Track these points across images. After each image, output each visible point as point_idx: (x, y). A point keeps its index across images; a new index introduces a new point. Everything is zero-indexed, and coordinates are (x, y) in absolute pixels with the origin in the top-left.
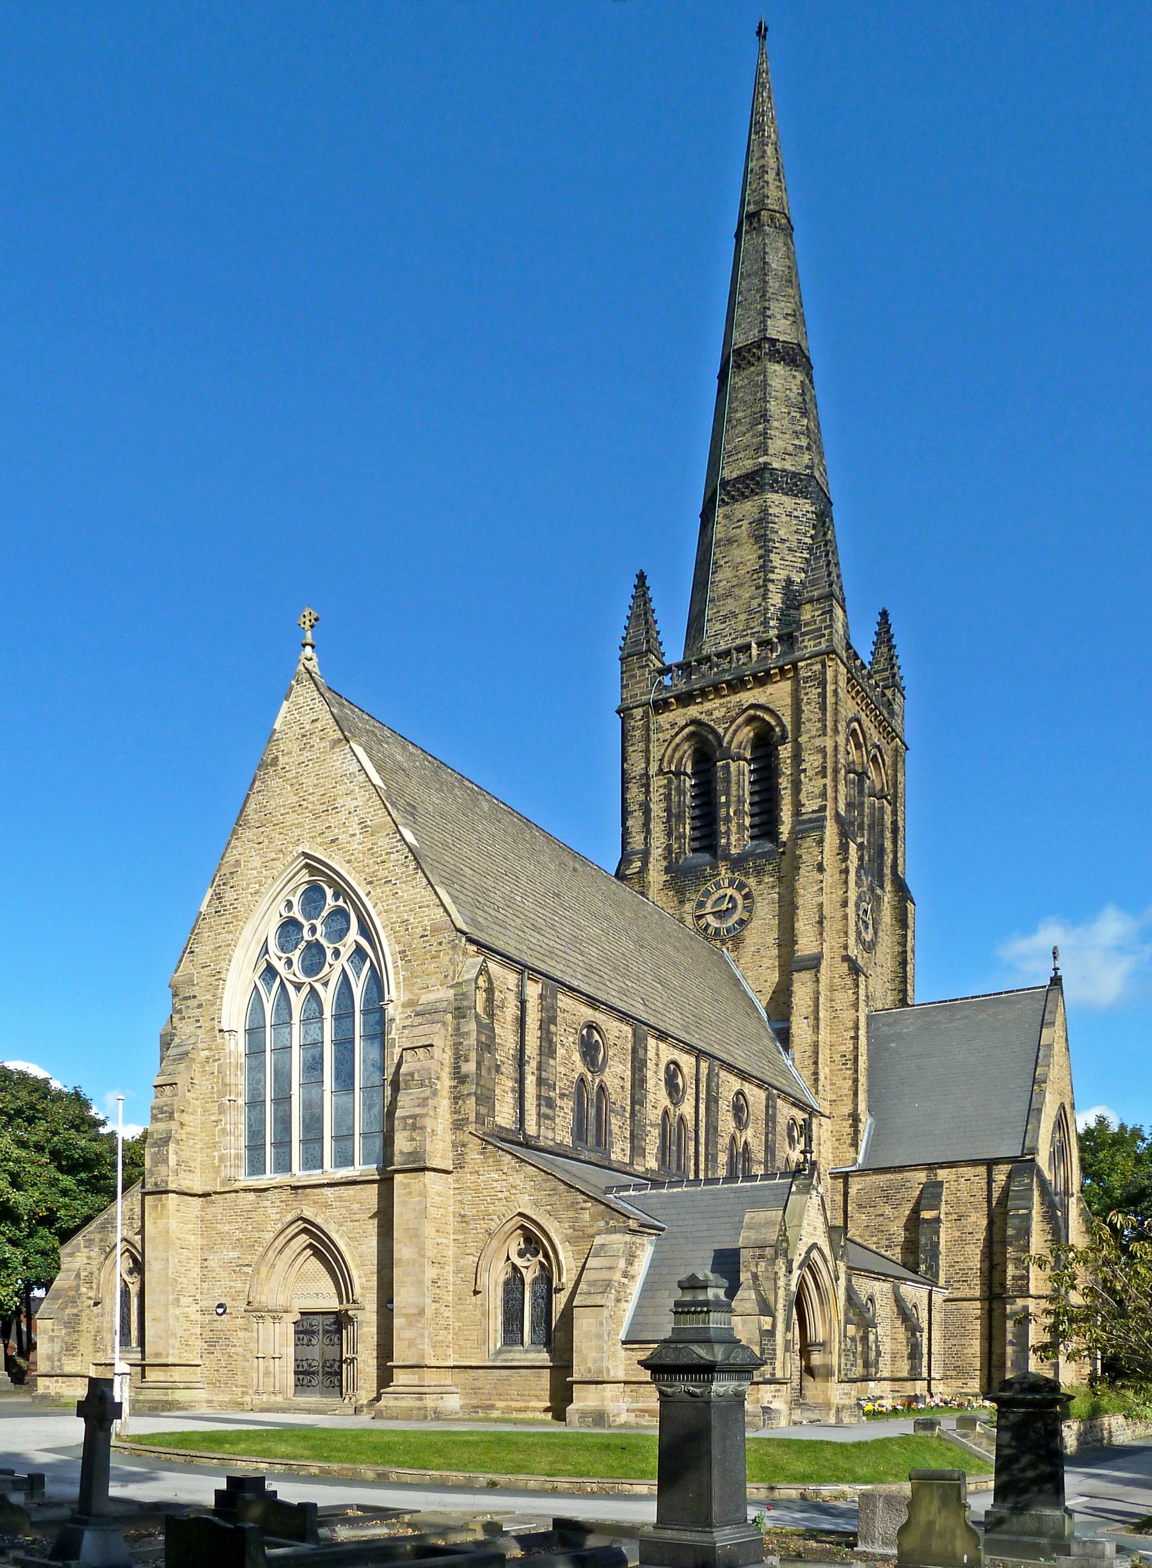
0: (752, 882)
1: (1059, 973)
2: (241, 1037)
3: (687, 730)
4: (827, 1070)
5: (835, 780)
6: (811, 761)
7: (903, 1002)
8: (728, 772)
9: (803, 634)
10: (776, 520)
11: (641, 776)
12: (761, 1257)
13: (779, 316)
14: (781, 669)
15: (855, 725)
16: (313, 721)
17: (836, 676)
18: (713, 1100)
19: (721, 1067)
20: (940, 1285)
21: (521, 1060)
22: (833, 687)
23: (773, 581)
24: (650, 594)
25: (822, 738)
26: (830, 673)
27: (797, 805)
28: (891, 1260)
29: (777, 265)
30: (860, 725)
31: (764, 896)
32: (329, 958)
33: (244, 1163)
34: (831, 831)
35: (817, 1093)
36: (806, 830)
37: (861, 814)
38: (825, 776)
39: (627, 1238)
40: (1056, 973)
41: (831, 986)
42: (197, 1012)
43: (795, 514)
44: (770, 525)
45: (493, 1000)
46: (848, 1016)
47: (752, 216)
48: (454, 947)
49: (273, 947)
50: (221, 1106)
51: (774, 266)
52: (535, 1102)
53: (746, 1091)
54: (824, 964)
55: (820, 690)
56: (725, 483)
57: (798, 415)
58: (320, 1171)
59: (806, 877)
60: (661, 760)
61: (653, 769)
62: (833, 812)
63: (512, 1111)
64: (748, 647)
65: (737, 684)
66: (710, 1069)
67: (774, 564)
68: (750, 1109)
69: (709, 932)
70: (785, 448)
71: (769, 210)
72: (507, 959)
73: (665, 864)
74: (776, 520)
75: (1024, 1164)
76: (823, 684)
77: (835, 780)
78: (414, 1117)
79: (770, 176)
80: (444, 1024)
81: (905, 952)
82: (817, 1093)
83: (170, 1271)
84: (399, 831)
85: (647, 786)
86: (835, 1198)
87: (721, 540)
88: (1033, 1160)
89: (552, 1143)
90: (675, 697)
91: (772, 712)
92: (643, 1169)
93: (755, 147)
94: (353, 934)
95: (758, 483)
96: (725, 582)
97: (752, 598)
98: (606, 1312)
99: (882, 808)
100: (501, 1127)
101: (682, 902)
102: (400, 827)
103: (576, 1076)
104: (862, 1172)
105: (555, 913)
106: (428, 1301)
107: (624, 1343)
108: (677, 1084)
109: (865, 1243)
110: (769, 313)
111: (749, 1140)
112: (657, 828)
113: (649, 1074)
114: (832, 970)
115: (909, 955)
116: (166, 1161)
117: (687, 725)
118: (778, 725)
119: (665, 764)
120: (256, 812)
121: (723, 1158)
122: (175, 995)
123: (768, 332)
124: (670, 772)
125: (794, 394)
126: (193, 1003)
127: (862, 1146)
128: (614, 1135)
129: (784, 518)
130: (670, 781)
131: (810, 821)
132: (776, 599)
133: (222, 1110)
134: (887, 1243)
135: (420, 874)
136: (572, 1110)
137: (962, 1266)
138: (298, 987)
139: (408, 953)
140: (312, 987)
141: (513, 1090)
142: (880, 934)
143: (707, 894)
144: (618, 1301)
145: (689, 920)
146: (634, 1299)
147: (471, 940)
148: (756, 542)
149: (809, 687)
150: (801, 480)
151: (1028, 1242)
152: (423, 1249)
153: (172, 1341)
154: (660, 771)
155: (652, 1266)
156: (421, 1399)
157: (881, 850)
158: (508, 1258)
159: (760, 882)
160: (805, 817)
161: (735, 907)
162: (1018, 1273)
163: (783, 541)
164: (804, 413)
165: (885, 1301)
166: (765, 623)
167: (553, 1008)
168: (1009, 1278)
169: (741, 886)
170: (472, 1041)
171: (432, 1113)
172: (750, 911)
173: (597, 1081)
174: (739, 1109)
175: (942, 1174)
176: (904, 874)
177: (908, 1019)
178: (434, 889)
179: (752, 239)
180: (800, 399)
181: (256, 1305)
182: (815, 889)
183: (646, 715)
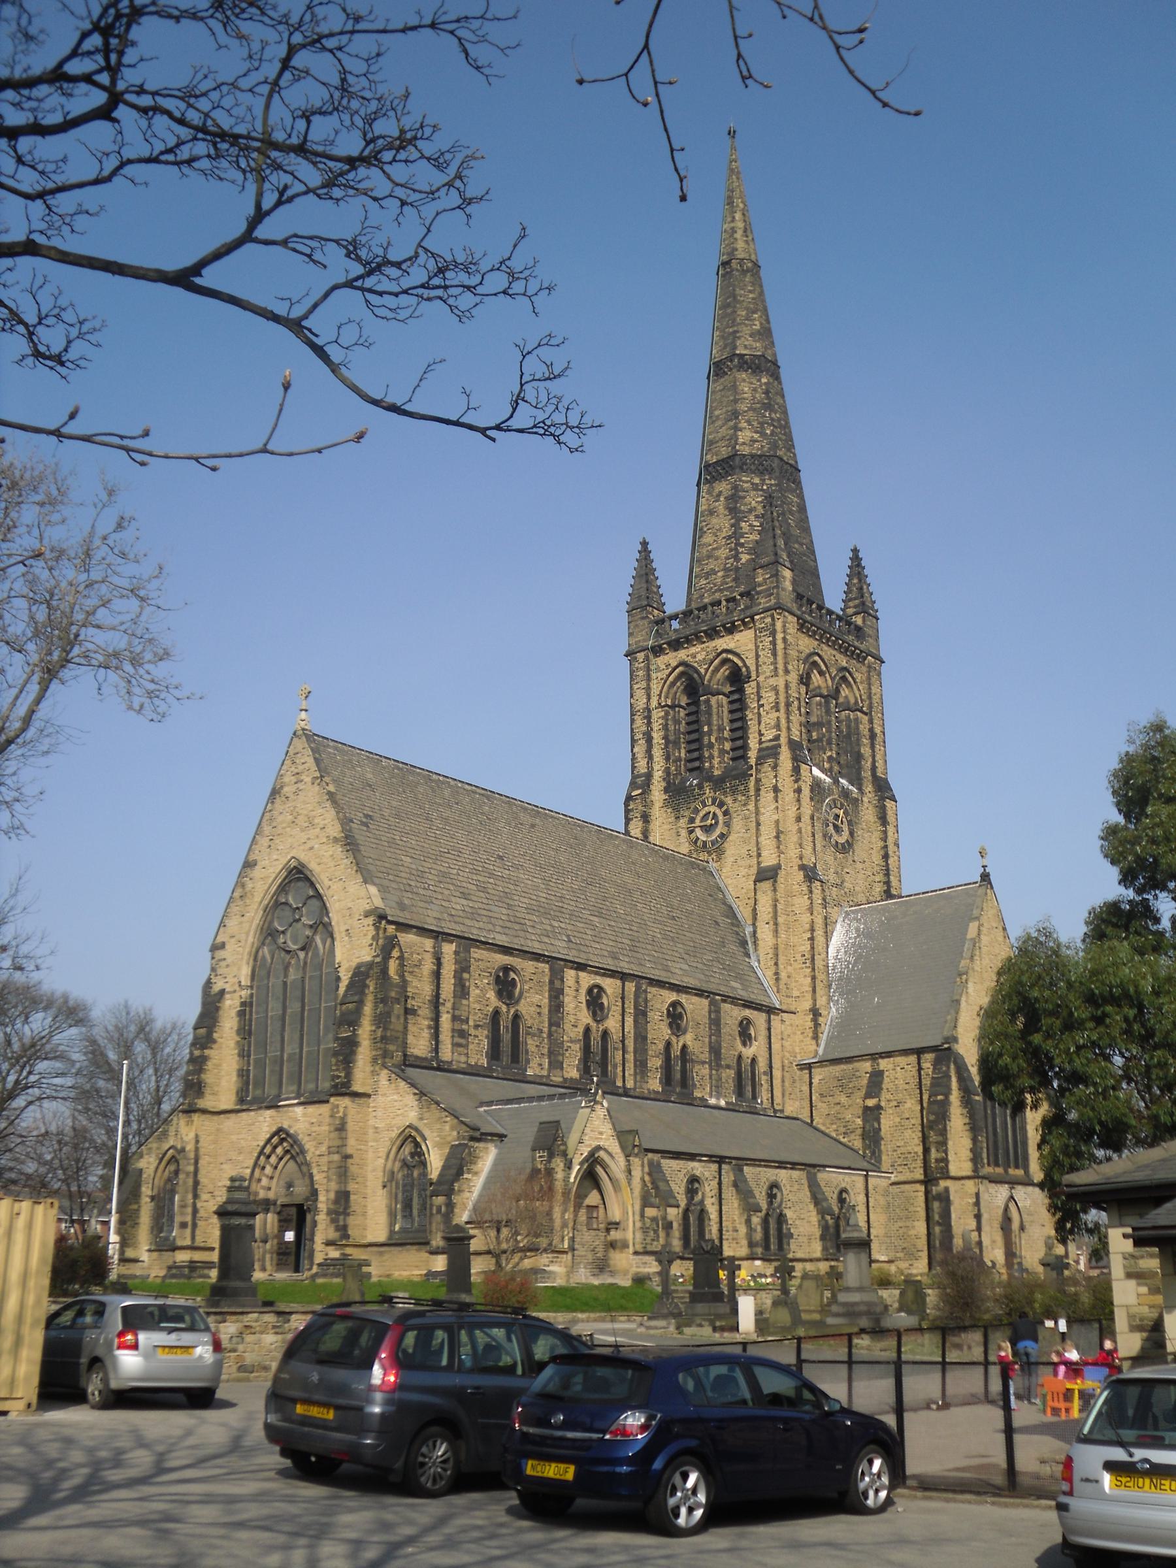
0: (729, 800)
3: (677, 671)
6: (768, 697)
8: (709, 706)
9: (758, 593)
11: (644, 709)
15: (817, 658)
18: (641, 1014)
22: (782, 635)
38: (778, 710)
46: (806, 918)
53: (683, 1001)
61: (654, 703)
63: (427, 1043)
64: (719, 603)
65: (712, 634)
66: (638, 988)
72: (422, 931)
76: (773, 633)
77: (788, 713)
81: (886, 847)
85: (648, 718)
88: (949, 1049)
89: (464, 1066)
92: (561, 1079)
97: (728, 558)
99: (856, 719)
104: (822, 1063)
112: (657, 753)
113: (566, 1000)
115: (891, 849)
117: (677, 667)
121: (655, 1063)
124: (667, 705)
126: (223, 964)
127: (823, 1038)
130: (667, 713)
131: (768, 748)
136: (487, 1037)
137: (903, 1150)
141: (429, 1027)
143: (696, 811)
145: (684, 833)
154: (660, 706)
157: (859, 757)
160: (764, 745)
161: (717, 823)
165: (796, 1187)
169: (721, 804)
172: (728, 826)
173: (512, 1011)
174: (675, 1017)
175: (884, 1064)
183: (647, 658)
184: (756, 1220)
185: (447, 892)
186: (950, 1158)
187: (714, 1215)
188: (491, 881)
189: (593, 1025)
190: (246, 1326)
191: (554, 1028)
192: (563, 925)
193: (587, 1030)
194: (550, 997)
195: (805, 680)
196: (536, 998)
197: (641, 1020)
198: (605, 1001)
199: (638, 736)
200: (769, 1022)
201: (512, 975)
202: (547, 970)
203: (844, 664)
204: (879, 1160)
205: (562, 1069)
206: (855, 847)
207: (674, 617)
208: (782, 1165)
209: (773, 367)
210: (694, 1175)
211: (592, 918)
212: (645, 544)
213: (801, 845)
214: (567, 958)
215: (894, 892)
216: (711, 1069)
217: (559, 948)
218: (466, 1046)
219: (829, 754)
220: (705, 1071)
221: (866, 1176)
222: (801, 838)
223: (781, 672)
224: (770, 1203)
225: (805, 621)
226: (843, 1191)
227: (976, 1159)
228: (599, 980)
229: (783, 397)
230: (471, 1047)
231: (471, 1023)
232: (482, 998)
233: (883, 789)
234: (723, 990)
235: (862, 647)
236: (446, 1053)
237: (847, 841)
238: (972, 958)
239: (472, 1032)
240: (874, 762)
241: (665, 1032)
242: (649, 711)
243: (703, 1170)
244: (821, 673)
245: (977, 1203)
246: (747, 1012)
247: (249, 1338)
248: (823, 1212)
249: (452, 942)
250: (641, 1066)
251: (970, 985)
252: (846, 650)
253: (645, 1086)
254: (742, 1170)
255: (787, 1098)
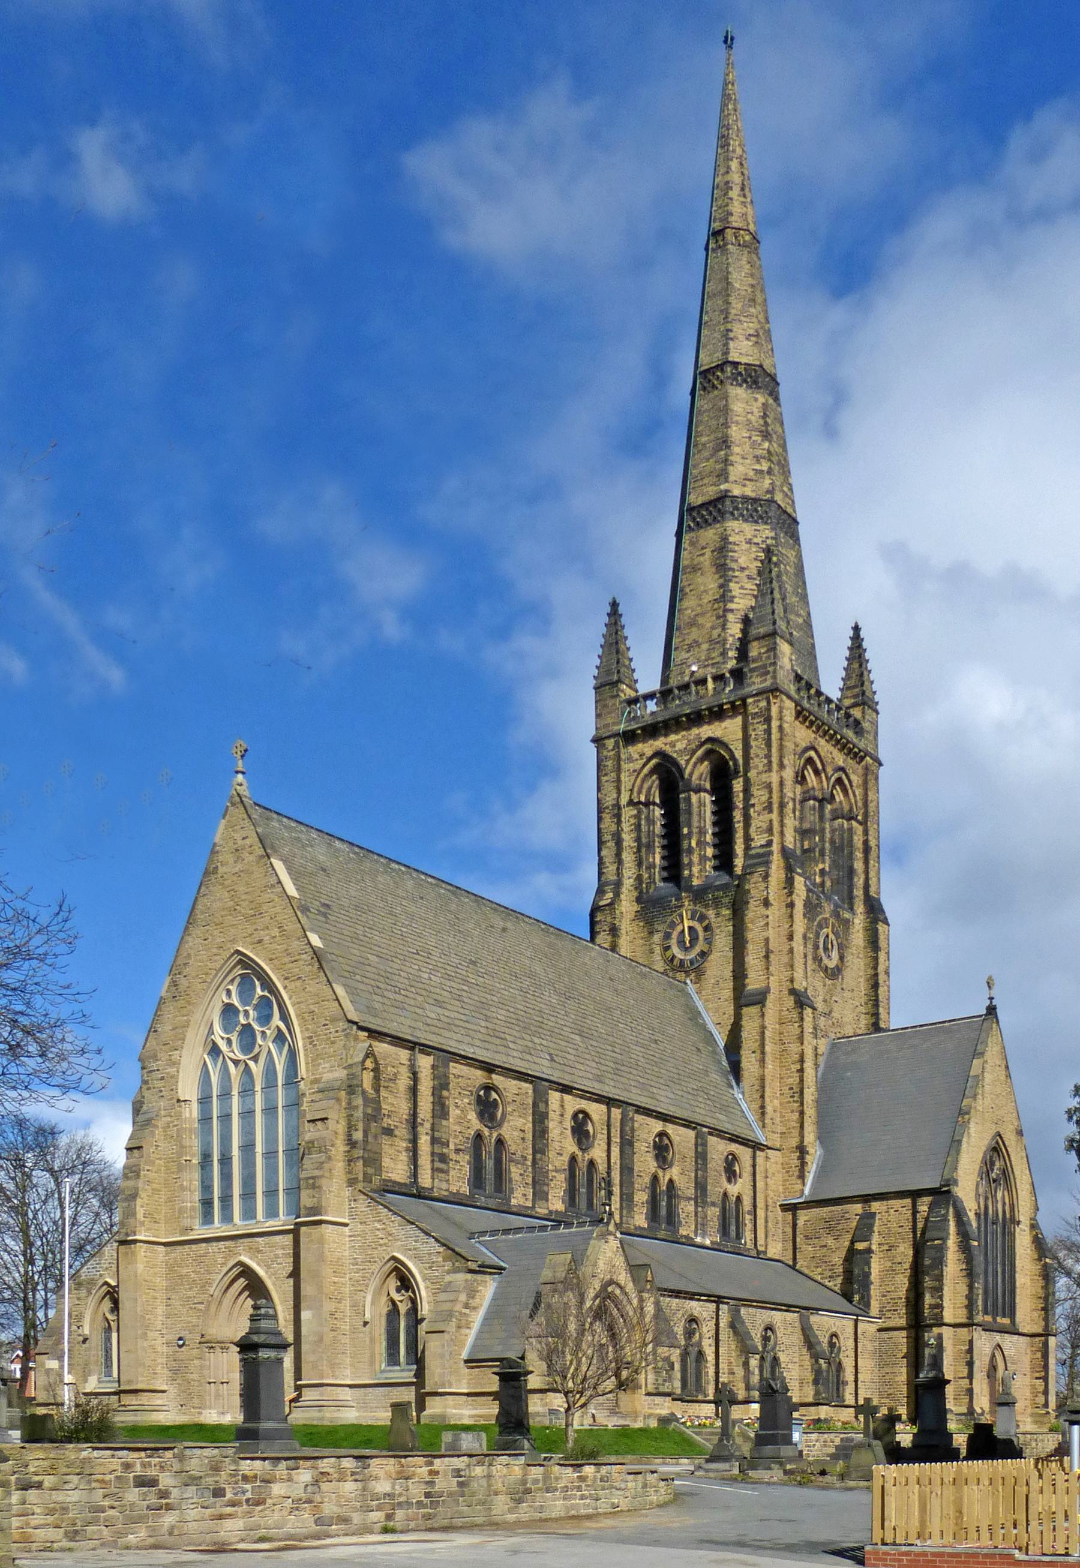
0: (711, 913)
1: (994, 1002)
2: (195, 1106)
4: (776, 1102)
5: (782, 815)
6: (759, 796)
7: (876, 1027)
9: (752, 670)
10: (736, 548)
11: (613, 805)
12: (555, 1291)
13: (741, 338)
14: (732, 703)
15: (812, 753)
16: (244, 838)
17: (781, 712)
18: (627, 1144)
19: (637, 1112)
20: (872, 1314)
21: (413, 1122)
22: (778, 723)
23: (732, 611)
24: (623, 620)
25: (767, 775)
26: (774, 710)
27: (747, 839)
28: (832, 1290)
29: (740, 284)
30: (817, 752)
31: (723, 928)
32: (259, 1041)
33: (198, 1214)
34: (777, 861)
35: (764, 1127)
36: (754, 865)
37: (822, 839)
39: (469, 1276)
40: (991, 1002)
41: (780, 1019)
42: (161, 1084)
43: (755, 540)
44: (730, 554)
45: (379, 1079)
46: (794, 1048)
47: (718, 234)
48: (346, 1035)
49: (217, 1028)
50: (180, 1164)
51: (737, 285)
52: (429, 1158)
53: (670, 1132)
54: (771, 998)
55: (765, 727)
56: (691, 509)
57: (759, 439)
58: (254, 1221)
59: (753, 911)
60: (631, 790)
61: (624, 799)
62: (780, 846)
63: (406, 1168)
64: (703, 682)
65: (696, 719)
67: (734, 593)
68: (675, 1147)
69: (675, 963)
70: (746, 474)
71: (733, 228)
72: (398, 1041)
73: (636, 894)
74: (736, 548)
75: (942, 1194)
76: (768, 720)
77: (782, 815)
78: (313, 1178)
79: (734, 193)
80: (338, 1100)
81: (876, 975)
82: (764, 1127)
83: (139, 1309)
84: (306, 936)
85: (618, 816)
86: (785, 1230)
87: (686, 567)
88: (949, 1192)
89: (446, 1193)
90: (642, 728)
91: (726, 746)
92: (546, 1212)
93: (721, 161)
94: (276, 1021)
95: (719, 510)
96: (690, 611)
98: (446, 1336)
99: (850, 829)
100: (395, 1182)
101: (651, 933)
102: (308, 933)
103: (473, 1133)
105: (465, 981)
106: (326, 1329)
107: (466, 1361)
108: (588, 1131)
109: (811, 1274)
110: (731, 335)
111: (675, 1178)
112: (628, 857)
113: (551, 1125)
114: (777, 1005)
115: (882, 978)
116: (134, 1214)
118: (731, 759)
119: (635, 794)
120: (203, 913)
121: (641, 1197)
122: (143, 1068)
123: (731, 354)
124: (640, 802)
125: (755, 418)
127: (810, 1178)
128: (514, 1183)
129: (745, 546)
130: (640, 812)
131: (759, 855)
132: (735, 629)
133: (180, 1169)
134: (830, 1274)
135: (322, 974)
136: (469, 1163)
138: (236, 1062)
139: (314, 1039)
140: (246, 1065)
141: (407, 1149)
142: (849, 958)
144: (459, 1327)
145: (658, 950)
146: (476, 1326)
147: (362, 1028)
148: (717, 572)
149: (758, 723)
150: (761, 506)
151: (942, 1272)
152: (321, 1286)
153: (140, 1370)
154: (631, 803)
155: (494, 1299)
156: (320, 1411)
157: (851, 872)
158: (389, 1294)
159: (718, 915)
160: (753, 852)
162: (933, 1302)
163: (742, 569)
164: (766, 435)
165: (790, 1330)
166: (724, 654)
167: (446, 1076)
168: (927, 1306)
169: (702, 918)
170: (359, 1114)
171: (327, 1174)
173: (495, 1135)
174: (662, 1149)
175: (876, 1206)
176: (879, 893)
177: (865, 1047)
178: (332, 987)
179: (717, 257)
180: (762, 422)
181: (207, 1338)
182: (762, 924)
183: (617, 745)
184: (754, 1362)
185: (420, 998)
186: (945, 1304)
187: (710, 1357)
188: (466, 988)
189: (579, 1153)
190: (322, 1473)
191: (538, 1156)
192: (544, 1042)
193: (573, 1159)
194: (534, 1122)
195: (800, 779)
196: (519, 1122)
197: (627, 1148)
198: (590, 1128)
199: (607, 837)
200: (754, 1157)
201: (494, 1095)
202: (530, 1091)
203: (841, 763)
204: (868, 1305)
205: (547, 1200)
206: (844, 973)
207: (650, 696)
208: (777, 1306)
209: (772, 384)
210: (692, 1315)
211: (573, 1036)
212: (856, 629)
213: (792, 966)
214: (552, 1078)
215: (882, 1025)
216: (696, 1206)
217: (543, 1068)
218: (446, 1172)
219: (821, 866)
220: (690, 1207)
221: (856, 1321)
222: (792, 959)
223: (775, 766)
224: (765, 1346)
225: (803, 709)
226: (834, 1335)
227: (970, 1306)
228: (584, 1104)
229: (782, 424)
230: (452, 1173)
231: (452, 1146)
232: (461, 1120)
233: (875, 911)
234: (709, 1121)
235: (862, 745)
236: (425, 1179)
237: (837, 966)
238: (975, 1097)
239: (453, 1156)
240: (867, 879)
241: (652, 1165)
242: (619, 808)
243: (702, 1310)
244: (817, 772)
245: (970, 1351)
246: (734, 1147)
247: (325, 1486)
248: (816, 1357)
249: (429, 1054)
250: (627, 1199)
251: (972, 1125)
252: (844, 746)
253: (631, 1221)
254: (739, 1311)
255: (770, 1239)
